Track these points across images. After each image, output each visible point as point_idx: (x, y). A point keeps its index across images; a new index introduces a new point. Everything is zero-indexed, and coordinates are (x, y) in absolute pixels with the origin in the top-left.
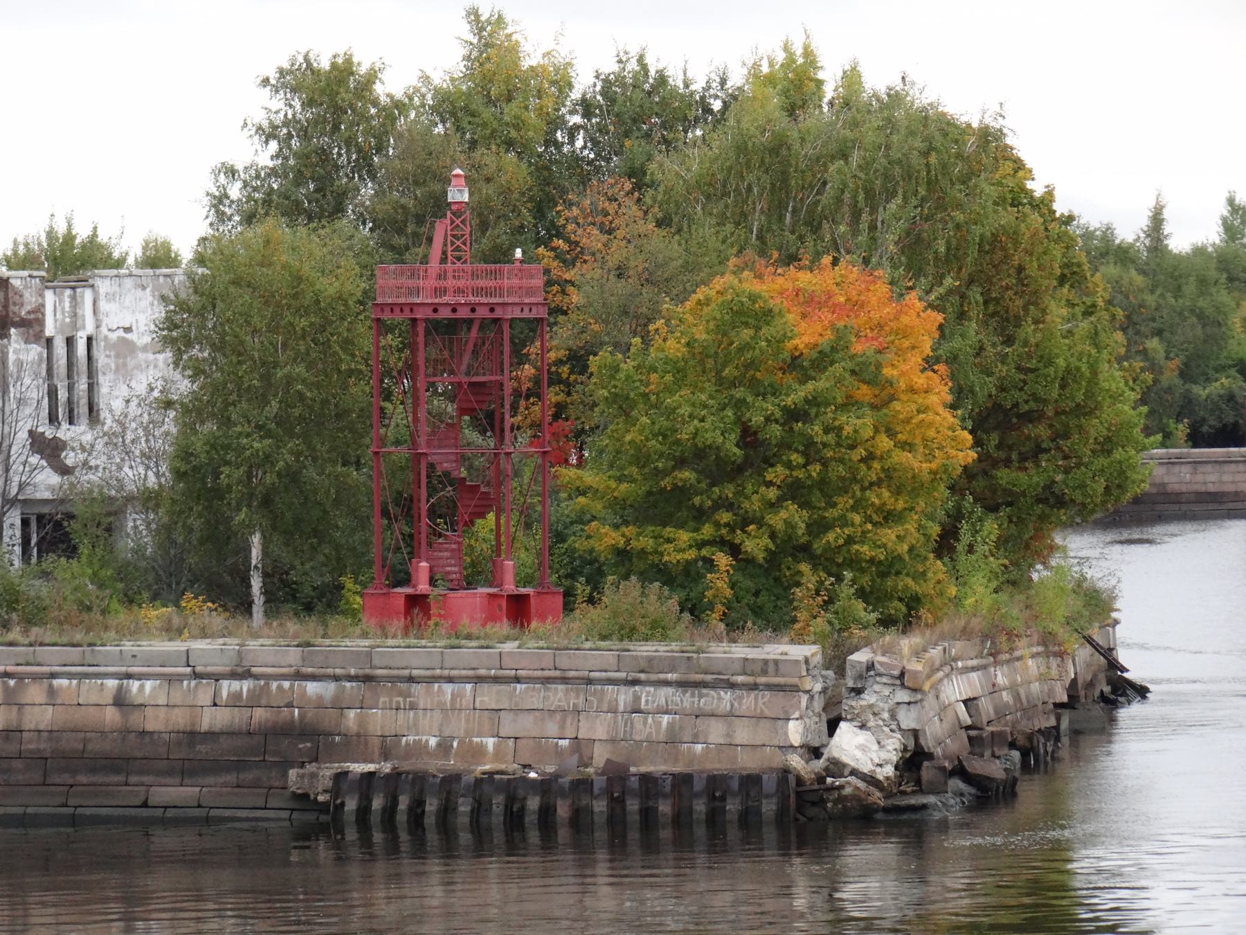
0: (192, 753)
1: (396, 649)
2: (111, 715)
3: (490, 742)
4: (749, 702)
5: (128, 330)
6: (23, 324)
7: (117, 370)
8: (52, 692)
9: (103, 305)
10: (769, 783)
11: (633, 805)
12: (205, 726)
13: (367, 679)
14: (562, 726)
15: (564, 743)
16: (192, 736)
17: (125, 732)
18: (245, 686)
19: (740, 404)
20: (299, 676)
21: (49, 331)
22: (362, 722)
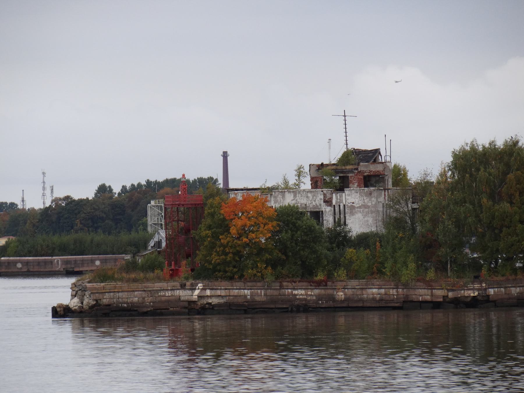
5: (353, 203)
7: (350, 213)
9: (347, 197)
21: (334, 203)
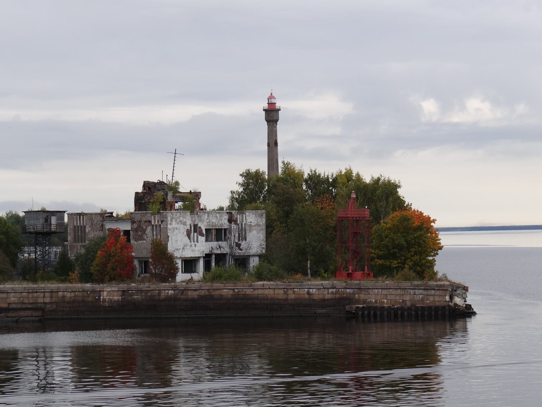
0: (323, 303)
1: (368, 283)
2: (307, 296)
3: (385, 301)
4: (438, 293)
6: (234, 221)
8: (294, 292)
9: (247, 218)
10: (447, 308)
11: (420, 313)
12: (326, 298)
13: (359, 289)
14: (400, 297)
15: (401, 301)
16: (324, 300)
17: (310, 299)
18: (334, 290)
19: (404, 236)
20: (346, 288)
21: (238, 222)
22: (359, 297)
